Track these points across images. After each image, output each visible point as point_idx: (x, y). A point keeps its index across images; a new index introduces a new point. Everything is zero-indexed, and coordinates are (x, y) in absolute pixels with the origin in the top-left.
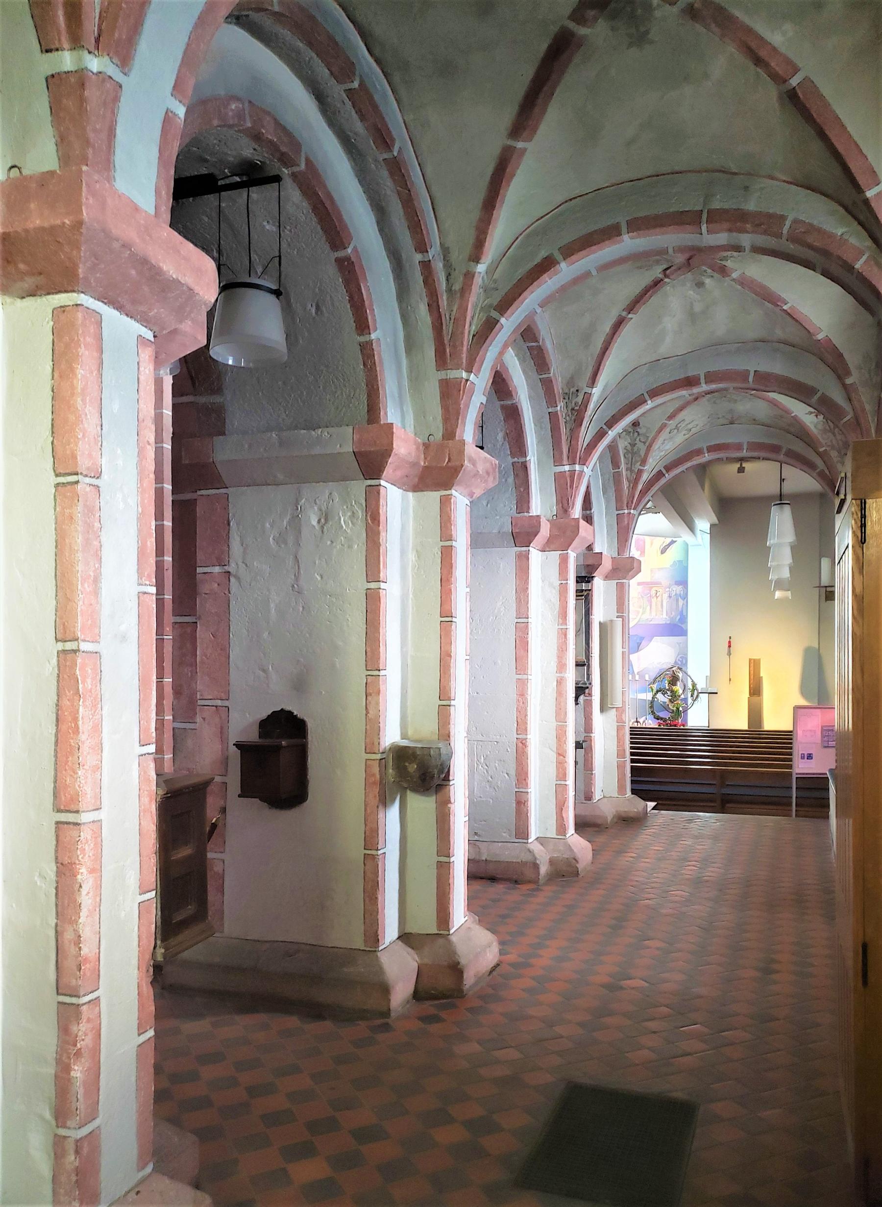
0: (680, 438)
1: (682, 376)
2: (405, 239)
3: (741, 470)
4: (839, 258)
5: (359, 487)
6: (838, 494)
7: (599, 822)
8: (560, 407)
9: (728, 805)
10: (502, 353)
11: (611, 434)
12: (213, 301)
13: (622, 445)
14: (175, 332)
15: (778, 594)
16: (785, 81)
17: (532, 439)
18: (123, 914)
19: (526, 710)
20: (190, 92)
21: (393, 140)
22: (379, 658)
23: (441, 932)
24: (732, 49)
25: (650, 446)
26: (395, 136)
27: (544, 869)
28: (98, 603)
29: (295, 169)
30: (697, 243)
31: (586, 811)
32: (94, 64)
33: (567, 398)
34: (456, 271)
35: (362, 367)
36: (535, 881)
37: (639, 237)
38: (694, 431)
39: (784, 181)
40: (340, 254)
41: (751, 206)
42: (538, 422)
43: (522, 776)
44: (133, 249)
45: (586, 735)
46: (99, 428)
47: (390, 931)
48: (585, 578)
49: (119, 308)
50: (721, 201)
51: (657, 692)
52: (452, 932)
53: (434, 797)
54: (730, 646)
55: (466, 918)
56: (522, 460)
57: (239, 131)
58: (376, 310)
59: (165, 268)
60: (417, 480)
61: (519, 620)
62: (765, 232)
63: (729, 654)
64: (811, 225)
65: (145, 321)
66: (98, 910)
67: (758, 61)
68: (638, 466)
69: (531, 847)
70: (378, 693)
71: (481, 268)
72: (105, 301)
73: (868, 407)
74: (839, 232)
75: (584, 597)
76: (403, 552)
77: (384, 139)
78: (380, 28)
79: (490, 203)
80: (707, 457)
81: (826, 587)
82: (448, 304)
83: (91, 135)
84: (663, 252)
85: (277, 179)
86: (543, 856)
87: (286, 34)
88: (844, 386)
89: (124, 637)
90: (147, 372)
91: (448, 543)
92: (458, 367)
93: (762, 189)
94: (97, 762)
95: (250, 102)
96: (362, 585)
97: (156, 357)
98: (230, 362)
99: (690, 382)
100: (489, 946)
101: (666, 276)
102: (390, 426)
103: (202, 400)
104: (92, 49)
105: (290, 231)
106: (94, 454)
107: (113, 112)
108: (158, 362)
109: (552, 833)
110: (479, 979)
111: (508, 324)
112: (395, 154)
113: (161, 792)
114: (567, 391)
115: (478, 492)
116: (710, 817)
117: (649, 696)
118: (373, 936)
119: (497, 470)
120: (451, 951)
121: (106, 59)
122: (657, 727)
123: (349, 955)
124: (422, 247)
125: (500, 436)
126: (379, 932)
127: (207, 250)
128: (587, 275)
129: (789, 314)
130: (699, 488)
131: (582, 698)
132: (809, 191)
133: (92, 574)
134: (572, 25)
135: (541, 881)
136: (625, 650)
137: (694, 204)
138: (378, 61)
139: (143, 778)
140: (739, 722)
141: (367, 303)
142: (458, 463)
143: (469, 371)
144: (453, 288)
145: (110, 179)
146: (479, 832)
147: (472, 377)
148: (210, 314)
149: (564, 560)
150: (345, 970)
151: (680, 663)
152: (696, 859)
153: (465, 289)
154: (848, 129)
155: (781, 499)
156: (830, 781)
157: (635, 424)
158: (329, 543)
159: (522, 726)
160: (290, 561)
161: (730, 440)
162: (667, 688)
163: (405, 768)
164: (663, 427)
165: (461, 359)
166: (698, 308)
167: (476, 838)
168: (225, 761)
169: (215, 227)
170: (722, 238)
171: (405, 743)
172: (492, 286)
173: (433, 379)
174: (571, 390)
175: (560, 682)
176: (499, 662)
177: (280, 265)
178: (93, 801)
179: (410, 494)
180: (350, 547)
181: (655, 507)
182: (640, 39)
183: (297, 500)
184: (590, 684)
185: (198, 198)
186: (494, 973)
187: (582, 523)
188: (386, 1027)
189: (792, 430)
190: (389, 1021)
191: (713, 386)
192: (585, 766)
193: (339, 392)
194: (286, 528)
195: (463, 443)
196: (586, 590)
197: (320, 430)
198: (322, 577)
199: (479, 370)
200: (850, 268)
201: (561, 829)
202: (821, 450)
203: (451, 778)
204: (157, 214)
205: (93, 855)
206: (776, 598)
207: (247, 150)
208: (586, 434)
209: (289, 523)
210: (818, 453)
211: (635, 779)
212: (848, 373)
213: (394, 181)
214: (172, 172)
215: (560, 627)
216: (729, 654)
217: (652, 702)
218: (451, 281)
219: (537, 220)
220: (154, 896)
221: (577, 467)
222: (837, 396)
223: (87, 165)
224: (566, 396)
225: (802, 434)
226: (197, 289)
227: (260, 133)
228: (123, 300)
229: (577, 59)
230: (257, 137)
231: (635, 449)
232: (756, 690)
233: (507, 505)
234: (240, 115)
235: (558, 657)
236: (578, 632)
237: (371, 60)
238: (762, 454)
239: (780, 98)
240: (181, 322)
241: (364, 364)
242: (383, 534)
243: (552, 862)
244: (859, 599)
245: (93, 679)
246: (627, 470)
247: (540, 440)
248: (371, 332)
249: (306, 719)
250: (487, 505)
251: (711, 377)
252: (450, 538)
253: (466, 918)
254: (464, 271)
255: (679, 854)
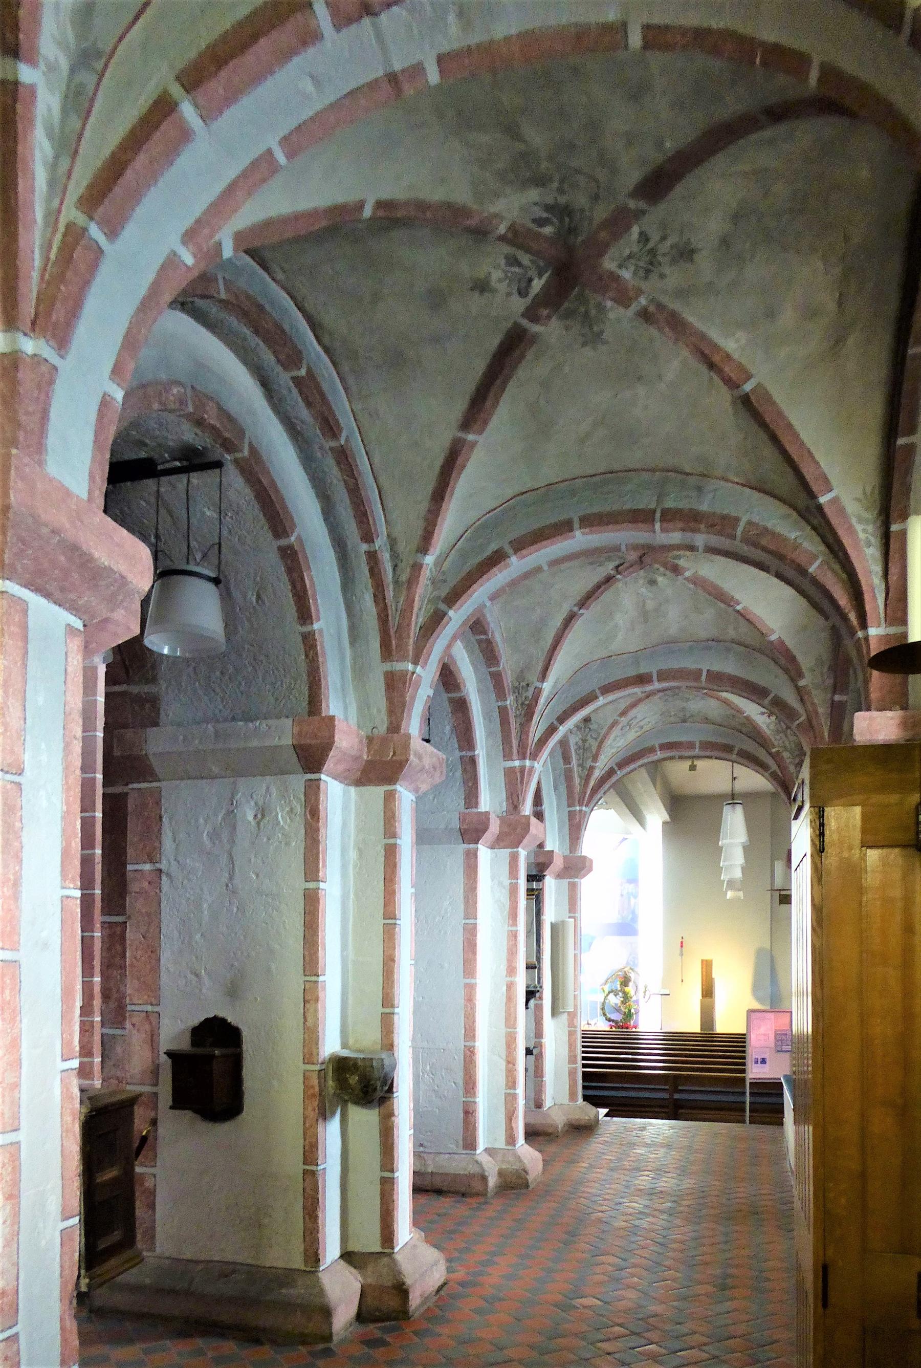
0: (632, 735)
1: (634, 673)
2: (351, 530)
3: (693, 768)
4: (793, 561)
5: (298, 781)
6: (795, 799)
7: (550, 1131)
8: (510, 701)
9: (680, 1111)
10: (449, 646)
11: (562, 730)
12: (147, 589)
13: (573, 741)
14: (106, 620)
15: (730, 894)
16: (738, 387)
17: (480, 732)
18: (43, 1243)
19: (474, 1016)
20: (128, 376)
21: (340, 429)
22: (318, 963)
23: (386, 1251)
24: (685, 353)
25: (602, 742)
26: (342, 425)
27: (492, 1181)
28: (17, 907)
29: (239, 455)
30: (649, 541)
31: (537, 1120)
32: (29, 346)
33: (516, 691)
34: (404, 562)
35: (303, 657)
36: (483, 1194)
37: (591, 532)
38: (646, 728)
39: (738, 483)
40: (283, 542)
41: (704, 507)
42: (487, 716)
43: (470, 1085)
44: (62, 535)
45: (536, 1040)
46: (22, 722)
47: (331, 1249)
48: (536, 876)
49: (47, 595)
50: (675, 501)
51: (609, 993)
52: (396, 1250)
53: (377, 1110)
54: (682, 946)
55: (412, 1235)
56: (470, 754)
57: (180, 416)
58: (319, 600)
59: (96, 555)
60: (359, 773)
61: (467, 921)
62: (720, 533)
63: (682, 955)
64: (766, 529)
65: (73, 609)
66: (16, 1239)
67: (711, 366)
68: (589, 763)
69: (479, 1158)
70: (317, 1000)
71: (429, 560)
72: (33, 588)
73: (821, 710)
74: (793, 536)
75: (536, 896)
76: (344, 851)
77: (330, 427)
78: (330, 318)
79: (439, 495)
80: (659, 755)
81: (780, 890)
82: (394, 596)
83: (23, 418)
84: (617, 549)
85: (218, 465)
86: (492, 1170)
87: (233, 322)
88: (797, 687)
89: (46, 944)
90: (75, 663)
91: (392, 841)
92: (404, 658)
93: (716, 490)
94: (15, 1080)
95: (193, 387)
96: (301, 885)
97: (86, 647)
98: (166, 651)
99: (642, 679)
100: (436, 1263)
101: (619, 573)
102: (332, 719)
103: (135, 689)
104: (28, 331)
105: (231, 518)
106: (16, 749)
107: (47, 395)
108: (87, 650)
109: (501, 1143)
110: (426, 1299)
111: (457, 616)
112: (343, 442)
113: (85, 1110)
114: (516, 684)
115: (424, 787)
116: (663, 1125)
117: (601, 998)
118: (313, 1256)
119: (444, 765)
120: (395, 1271)
121: (42, 342)
122: (608, 1029)
123: (287, 1277)
124: (368, 537)
125: (448, 729)
126: (320, 1251)
127: (144, 538)
128: (539, 569)
129: (742, 615)
130: (652, 786)
131: (532, 1003)
132: (762, 495)
133: (12, 877)
134: (525, 322)
135: (489, 1195)
136: (576, 952)
137: (646, 501)
138: (327, 350)
139: (66, 1095)
140: (693, 1026)
141: (310, 593)
142: (403, 758)
143: (416, 662)
144: (400, 580)
145: (41, 463)
146: (425, 1143)
147: (419, 669)
148: (145, 603)
149: (514, 858)
150: (284, 1291)
151: (631, 963)
152: (650, 1168)
153: (412, 581)
154: (801, 436)
155: (733, 798)
156: (785, 1087)
157: (587, 720)
158: (265, 840)
159: (470, 1032)
160: (224, 860)
161: (684, 738)
162: (619, 989)
163: (346, 1080)
164: (614, 724)
165: (408, 651)
166: (650, 605)
167: (422, 1149)
168: (155, 1071)
169: (153, 511)
170: (675, 537)
171: (345, 1053)
172: (441, 578)
173: (378, 670)
174: (521, 684)
175: (510, 986)
176: (446, 965)
177: (220, 552)
178: (11, 1121)
179: (352, 789)
180: (288, 844)
181: (606, 803)
182: (594, 339)
183: (232, 794)
184: (541, 987)
185: (136, 483)
186: (442, 1293)
187: (533, 820)
188: (328, 1353)
189: (744, 730)
190: (332, 1345)
191: (665, 685)
192: (536, 1073)
193: (279, 683)
194: (221, 824)
195: (408, 737)
196: (537, 889)
197: (259, 722)
198: (257, 876)
199: (426, 663)
200: (803, 572)
201: (511, 1139)
202: (774, 750)
203: (394, 1090)
204: (90, 499)
205: (11, 1180)
206: (728, 898)
207: (189, 435)
208: (537, 729)
209: (224, 819)
210: (770, 754)
211: (586, 1084)
212: (800, 675)
213: (341, 469)
214: (108, 456)
215: (510, 928)
216: (682, 955)
217: (604, 1003)
218: (398, 573)
219: (488, 513)
220: (78, 1221)
221: (528, 763)
222: (790, 698)
223: (17, 448)
224: (516, 690)
225: (755, 734)
226: (130, 577)
227: (202, 418)
228: (52, 587)
229: (530, 355)
230: (199, 423)
231: (587, 745)
232: (708, 992)
233: (455, 801)
234: (182, 402)
235: (508, 960)
236: (528, 933)
237: (319, 348)
238: (715, 753)
239: (734, 403)
240: (112, 611)
241: (307, 656)
242: (322, 831)
243: (501, 1173)
244: (817, 909)
245: (12, 989)
246: (579, 766)
247: (489, 734)
248: (314, 622)
249: (240, 1026)
250: (434, 800)
251: (663, 676)
252: (394, 835)
253: (412, 1235)
254: (411, 562)
255: (632, 1164)
